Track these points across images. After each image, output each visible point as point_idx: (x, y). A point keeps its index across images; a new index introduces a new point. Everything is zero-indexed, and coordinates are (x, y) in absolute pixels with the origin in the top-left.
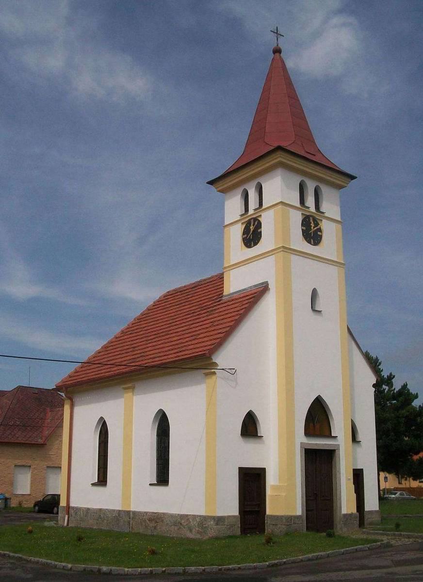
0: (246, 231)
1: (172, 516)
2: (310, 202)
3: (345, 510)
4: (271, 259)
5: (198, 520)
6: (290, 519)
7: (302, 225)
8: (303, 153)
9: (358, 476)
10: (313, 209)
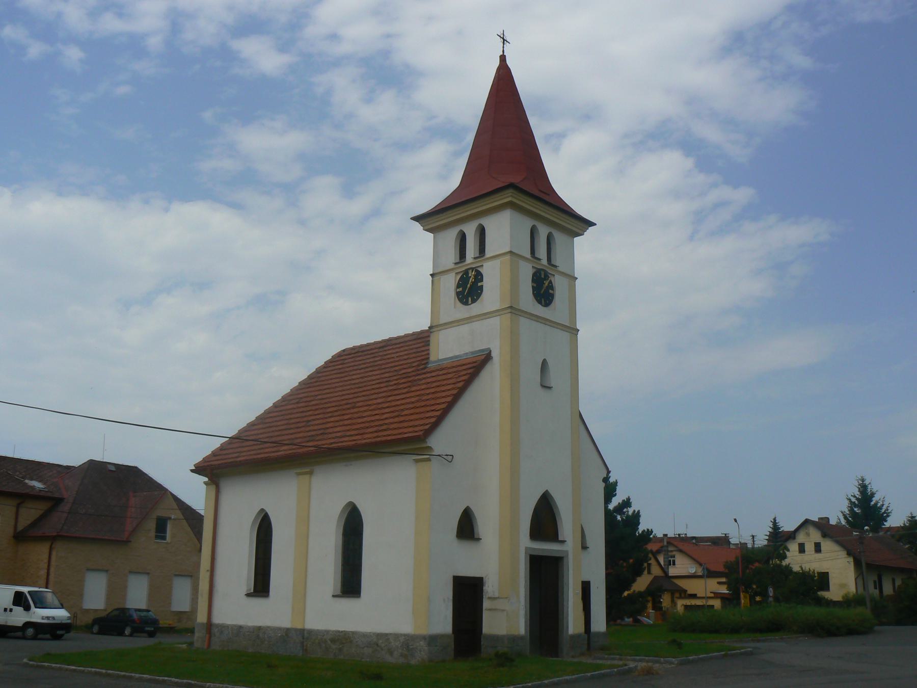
0: (463, 282)
1: (364, 635)
2: (542, 252)
3: (571, 631)
4: (496, 321)
5: (402, 639)
6: (514, 639)
7: (533, 281)
8: (536, 193)
9: (586, 588)
10: (544, 261)
